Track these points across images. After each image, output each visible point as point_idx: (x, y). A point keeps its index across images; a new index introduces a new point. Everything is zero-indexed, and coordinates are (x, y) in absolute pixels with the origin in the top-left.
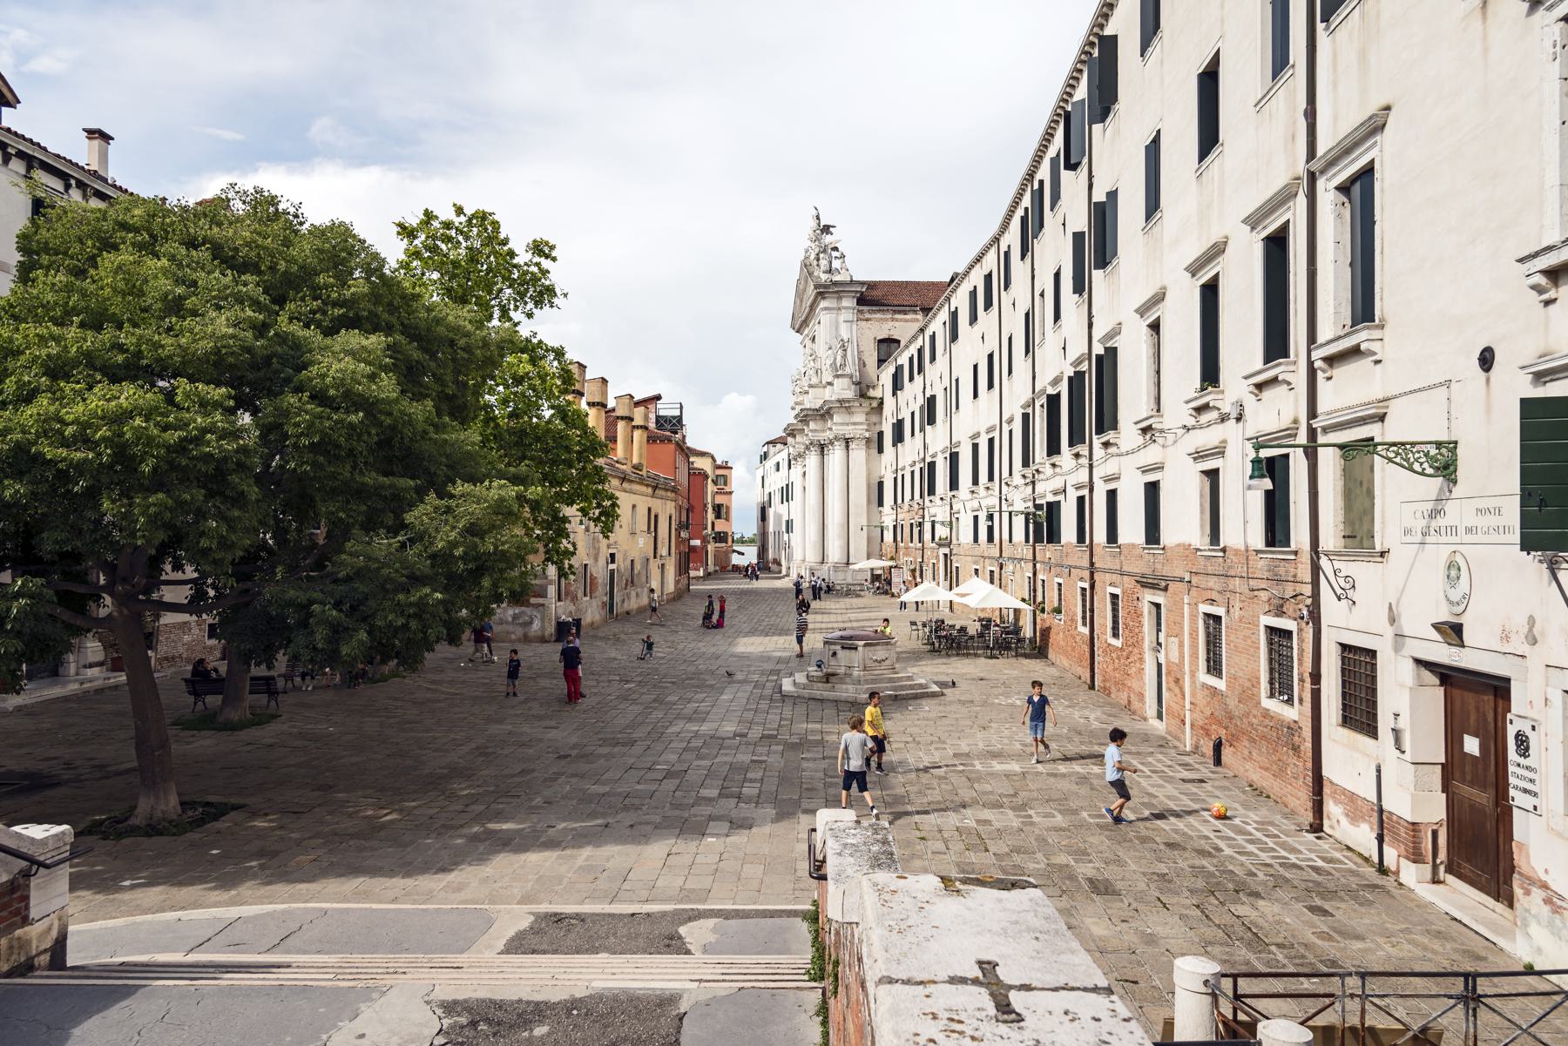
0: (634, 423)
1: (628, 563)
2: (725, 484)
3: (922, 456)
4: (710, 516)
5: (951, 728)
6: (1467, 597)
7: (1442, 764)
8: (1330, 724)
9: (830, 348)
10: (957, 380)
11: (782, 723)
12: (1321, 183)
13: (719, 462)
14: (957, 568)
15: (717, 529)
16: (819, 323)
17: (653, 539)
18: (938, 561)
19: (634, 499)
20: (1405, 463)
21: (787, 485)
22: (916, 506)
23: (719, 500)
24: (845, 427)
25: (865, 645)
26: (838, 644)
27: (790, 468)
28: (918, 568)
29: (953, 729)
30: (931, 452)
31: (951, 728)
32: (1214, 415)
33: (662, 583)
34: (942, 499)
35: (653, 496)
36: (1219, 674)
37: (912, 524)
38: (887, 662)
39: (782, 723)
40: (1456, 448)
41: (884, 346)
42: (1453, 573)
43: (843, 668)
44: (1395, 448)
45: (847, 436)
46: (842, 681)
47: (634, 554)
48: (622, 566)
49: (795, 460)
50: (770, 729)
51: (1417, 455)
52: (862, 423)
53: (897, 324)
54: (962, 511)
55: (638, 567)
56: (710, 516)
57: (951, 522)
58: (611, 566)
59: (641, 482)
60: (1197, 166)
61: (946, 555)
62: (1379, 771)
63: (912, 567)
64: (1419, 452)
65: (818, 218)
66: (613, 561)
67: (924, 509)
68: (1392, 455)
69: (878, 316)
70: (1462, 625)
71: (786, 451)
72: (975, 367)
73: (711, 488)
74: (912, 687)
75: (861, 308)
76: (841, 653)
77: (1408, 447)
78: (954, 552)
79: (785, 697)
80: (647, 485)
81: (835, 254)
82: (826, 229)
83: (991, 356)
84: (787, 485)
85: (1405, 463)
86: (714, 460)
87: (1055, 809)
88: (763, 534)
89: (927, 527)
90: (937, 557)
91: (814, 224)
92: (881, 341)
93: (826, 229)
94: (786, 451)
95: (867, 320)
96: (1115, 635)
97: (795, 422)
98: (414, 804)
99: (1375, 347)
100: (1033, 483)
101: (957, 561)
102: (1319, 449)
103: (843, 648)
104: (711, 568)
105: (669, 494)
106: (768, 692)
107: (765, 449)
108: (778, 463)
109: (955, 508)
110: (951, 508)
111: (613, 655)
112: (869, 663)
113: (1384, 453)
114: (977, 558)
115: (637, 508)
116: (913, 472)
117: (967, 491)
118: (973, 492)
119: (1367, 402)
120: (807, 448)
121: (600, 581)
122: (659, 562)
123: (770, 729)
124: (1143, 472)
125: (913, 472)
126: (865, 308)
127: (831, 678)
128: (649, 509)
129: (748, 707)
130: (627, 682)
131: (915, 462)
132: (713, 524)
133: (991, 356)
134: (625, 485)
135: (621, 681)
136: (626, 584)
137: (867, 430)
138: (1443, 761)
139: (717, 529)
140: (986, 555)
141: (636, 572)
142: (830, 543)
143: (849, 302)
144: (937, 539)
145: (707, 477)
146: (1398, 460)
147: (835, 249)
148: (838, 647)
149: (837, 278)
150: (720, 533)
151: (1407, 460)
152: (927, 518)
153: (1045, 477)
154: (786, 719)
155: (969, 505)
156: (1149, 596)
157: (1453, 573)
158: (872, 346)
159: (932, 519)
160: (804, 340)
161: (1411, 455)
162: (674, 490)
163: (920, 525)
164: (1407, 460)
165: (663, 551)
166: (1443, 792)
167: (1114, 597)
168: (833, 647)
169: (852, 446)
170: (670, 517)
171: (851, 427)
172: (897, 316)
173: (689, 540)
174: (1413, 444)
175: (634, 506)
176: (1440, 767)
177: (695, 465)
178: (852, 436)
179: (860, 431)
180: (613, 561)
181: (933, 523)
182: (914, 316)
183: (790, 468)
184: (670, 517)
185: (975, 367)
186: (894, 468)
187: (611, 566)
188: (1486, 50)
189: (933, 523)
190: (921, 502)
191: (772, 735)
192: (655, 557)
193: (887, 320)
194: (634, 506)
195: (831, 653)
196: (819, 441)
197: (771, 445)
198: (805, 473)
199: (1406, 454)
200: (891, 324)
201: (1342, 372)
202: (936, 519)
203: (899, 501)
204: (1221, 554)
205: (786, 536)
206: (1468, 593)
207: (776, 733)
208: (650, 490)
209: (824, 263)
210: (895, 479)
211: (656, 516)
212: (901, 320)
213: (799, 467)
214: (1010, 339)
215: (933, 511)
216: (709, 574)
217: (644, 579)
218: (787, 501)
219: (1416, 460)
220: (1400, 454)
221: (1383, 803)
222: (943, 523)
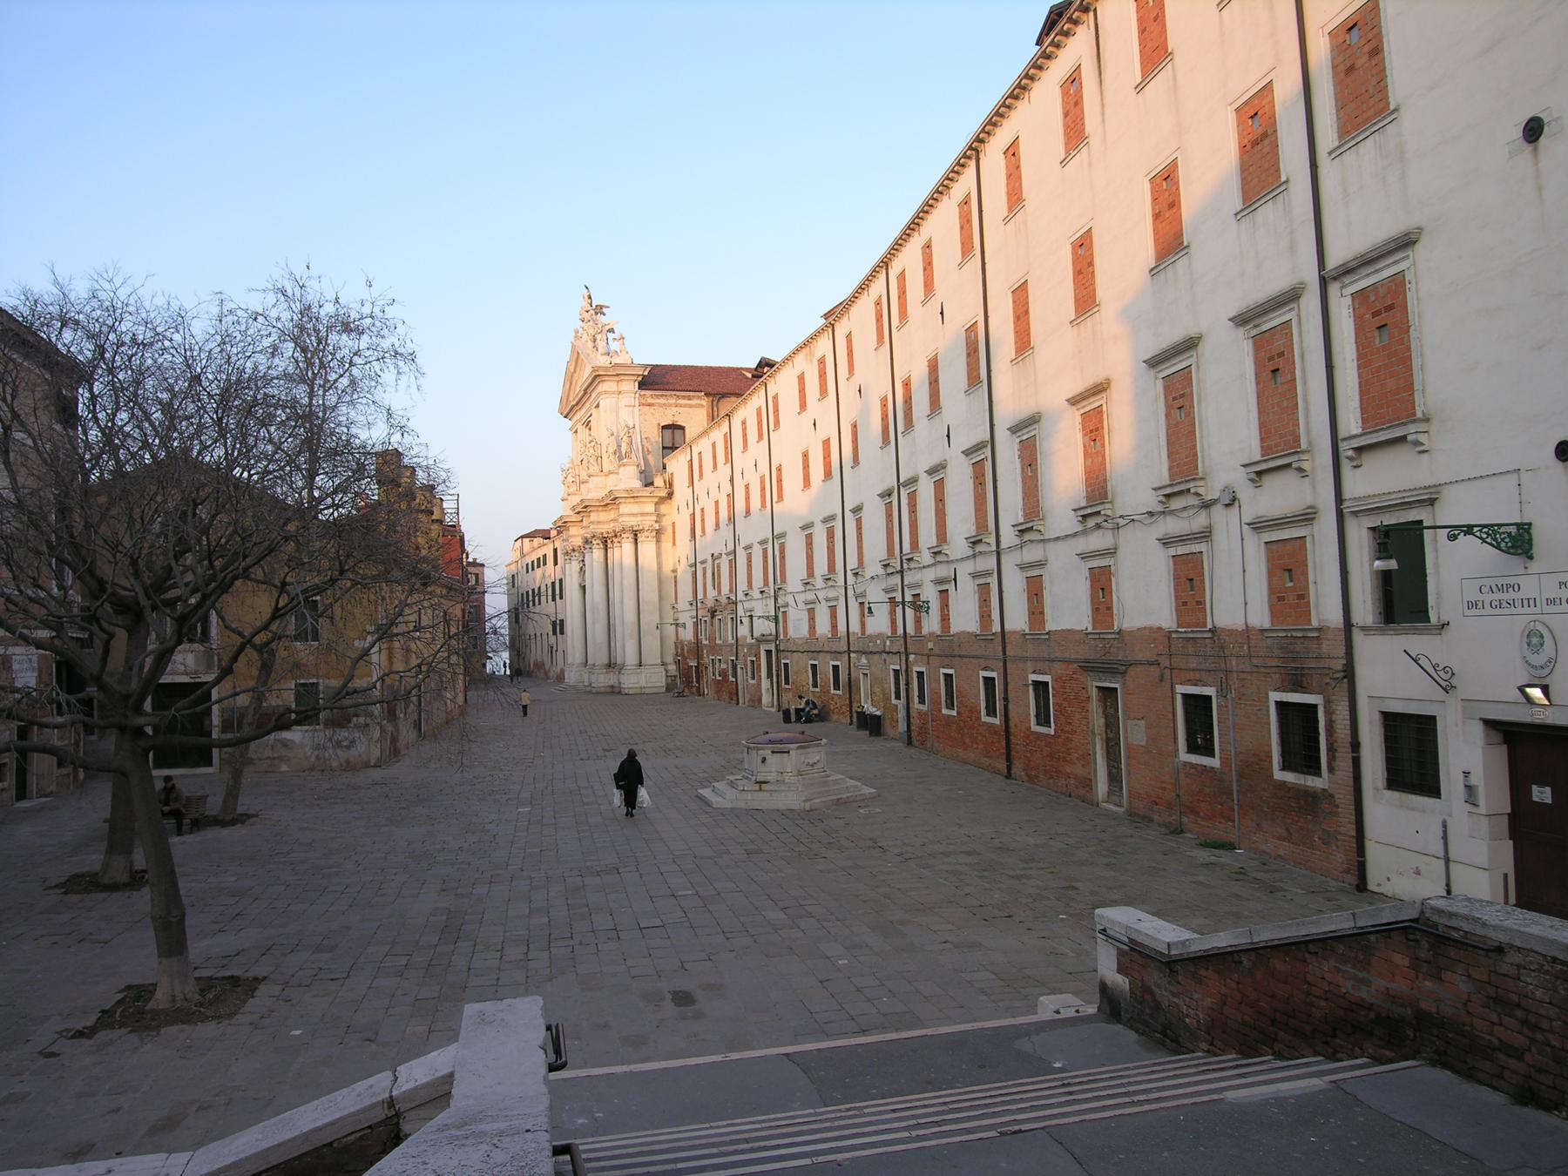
0: (434, 517)
6: (1552, 662)
7: (1509, 814)
8: (1376, 789)
9: (612, 435)
10: (779, 469)
12: (1334, 289)
14: (786, 665)
16: (598, 406)
20: (1494, 543)
24: (632, 518)
25: (799, 748)
26: (768, 748)
32: (1192, 500)
38: (819, 766)
40: (1530, 528)
41: (668, 432)
42: (1535, 640)
43: (775, 774)
44: (1486, 530)
45: (635, 529)
51: (1503, 536)
52: (651, 514)
53: (681, 410)
54: (792, 602)
57: (776, 618)
60: (960, 261)
61: (769, 652)
62: (1445, 826)
64: (1504, 533)
65: (590, 297)
68: (1484, 536)
69: (662, 401)
72: (805, 456)
75: (643, 392)
76: (771, 759)
77: (1496, 528)
81: (610, 335)
82: (599, 310)
83: (826, 443)
85: (1494, 543)
90: (757, 655)
91: (584, 304)
92: (663, 427)
93: (599, 310)
95: (650, 405)
97: (572, 513)
98: (421, 959)
99: (1423, 438)
100: (901, 572)
102: (1425, 531)
108: (545, 556)
110: (776, 600)
112: (804, 768)
113: (1478, 534)
119: (1412, 487)
120: (587, 541)
124: (1082, 558)
126: (648, 393)
131: (721, 554)
133: (826, 443)
137: (656, 522)
138: (1509, 811)
143: (630, 386)
146: (1489, 540)
147: (611, 331)
149: (616, 360)
151: (1495, 540)
152: (740, 612)
153: (917, 565)
156: (1093, 684)
157: (1535, 640)
158: (656, 433)
160: (573, 426)
161: (1498, 536)
164: (1495, 540)
166: (1510, 839)
167: (1040, 687)
168: (761, 752)
169: (641, 538)
171: (640, 518)
172: (680, 401)
174: (1500, 525)
176: (1506, 816)
178: (641, 528)
179: (649, 521)
182: (698, 402)
185: (805, 456)
188: (1540, 189)
193: (670, 405)
196: (602, 534)
197: (526, 541)
199: (1495, 535)
200: (675, 409)
201: (1372, 461)
203: (700, 596)
204: (1209, 635)
205: (552, 639)
206: (1554, 658)
209: (601, 344)
212: (686, 406)
214: (855, 426)
219: (1503, 540)
220: (1490, 535)
221: (1449, 856)
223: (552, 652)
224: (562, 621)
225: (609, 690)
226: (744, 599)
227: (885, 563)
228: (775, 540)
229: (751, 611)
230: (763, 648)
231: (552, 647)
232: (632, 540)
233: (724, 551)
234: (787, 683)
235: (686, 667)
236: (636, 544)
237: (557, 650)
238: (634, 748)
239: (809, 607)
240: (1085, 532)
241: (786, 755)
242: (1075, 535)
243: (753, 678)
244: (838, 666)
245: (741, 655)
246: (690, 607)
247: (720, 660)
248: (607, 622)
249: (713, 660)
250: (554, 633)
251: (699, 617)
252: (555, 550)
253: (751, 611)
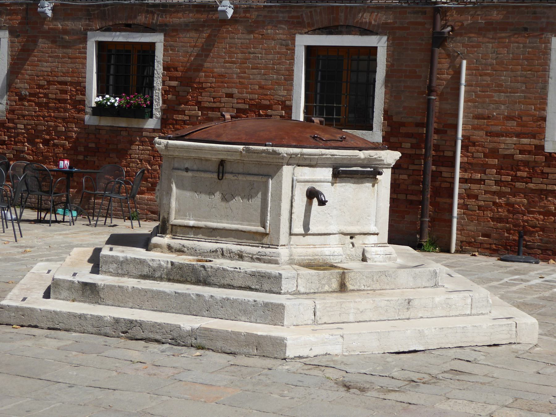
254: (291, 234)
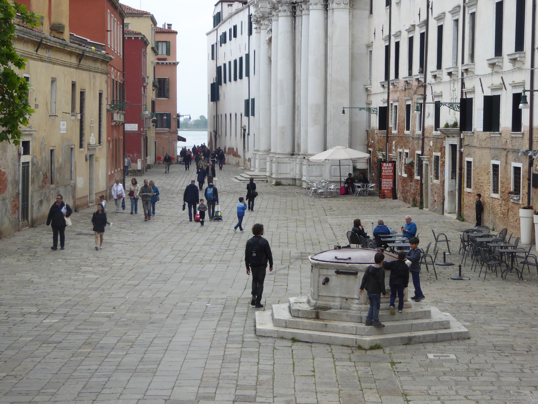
1: (46, 154)
2: (168, 52)
3: (424, 17)
4: (150, 94)
5: (491, 388)
11: (261, 378)
13: (160, 25)
14: (469, 163)
15: (158, 111)
17: (78, 124)
18: (443, 154)
19: (58, 71)
21: (248, 56)
22: (415, 83)
23: (162, 74)
27: (250, 33)
28: (416, 162)
29: (495, 388)
30: (436, 12)
31: (491, 388)
33: (91, 179)
34: (450, 74)
35: (78, 67)
36: (470, 187)
37: (408, 107)
39: (261, 378)
43: (338, 300)
46: (336, 317)
47: (55, 142)
48: (39, 157)
49: (257, 22)
50: (245, 387)
55: (59, 158)
56: (150, 94)
58: (25, 158)
59: (63, 50)
61: (453, 147)
63: (408, 161)
66: (26, 152)
67: (425, 87)
70: (380, 107)
71: (245, 13)
73: (150, 58)
74: (430, 326)
76: (335, 280)
78: (466, 143)
79: (260, 335)
80: (71, 53)
84: (248, 56)
86: (154, 22)
87: (70, 46)
88: (217, 118)
89: (430, 109)
94: (245, 13)
96: (496, 191)
101: (469, 155)
103: (338, 272)
104: (150, 159)
105: (98, 65)
106: (237, 331)
107: (219, 9)
108: (235, 27)
109: (468, 85)
111: (28, 276)
114: (497, 152)
115: (58, 83)
116: (411, 40)
117: (486, 64)
118: (493, 65)
121: (10, 178)
122: (85, 151)
123: (245, 387)
125: (411, 40)
127: (322, 313)
128: (74, 85)
129: (212, 353)
130: (49, 315)
131: (414, 26)
132: (153, 103)
134: (41, 52)
135: (39, 313)
136: (44, 181)
139: (158, 111)
140: (509, 146)
141: (56, 165)
142: (303, 129)
144: (442, 125)
145: (145, 43)
148: (331, 273)
150: (162, 115)
152: (429, 99)
154: (266, 372)
155: (487, 83)
159: (436, 100)
162: (105, 61)
163: (421, 108)
165: (92, 138)
168: (324, 272)
170: (100, 95)
173: (123, 124)
175: (53, 81)
177: (131, 28)
180: (26, 152)
181: (438, 106)
183: (250, 33)
184: (100, 95)
186: (386, 33)
187: (25, 158)
189: (438, 106)
190: (421, 78)
191: (249, 397)
192: (81, 146)
194: (53, 81)
195: (322, 280)
198: (270, 40)
202: (443, 100)
203: (392, 76)
205: (245, 119)
207: (253, 393)
208: (74, 60)
210: (388, 48)
211: (82, 94)
213: (263, 33)
215: (437, 89)
216: (149, 167)
217: (67, 176)
218: (248, 75)
222: (451, 105)
223: (244, 136)
224: (253, 100)
225: (291, 182)
226: (433, 81)
227: (492, 62)
228: (467, 9)
229: (438, 96)
230: (448, 142)
231: (245, 130)
232: (289, 13)
233: (417, 23)
234: (469, 186)
235: (376, 160)
236: (326, 10)
237: (249, 134)
238: (476, 194)
239: (255, 152)
240: (241, 127)
241: (352, 277)
242: (241, 124)
243: (437, 178)
244: (520, 168)
245: (427, 148)
246: (382, 90)
247: (407, 153)
248: (291, 103)
249: (401, 153)
250: (247, 114)
251: (391, 102)
252: (250, 16)
253: (438, 96)
254: (319, 296)
